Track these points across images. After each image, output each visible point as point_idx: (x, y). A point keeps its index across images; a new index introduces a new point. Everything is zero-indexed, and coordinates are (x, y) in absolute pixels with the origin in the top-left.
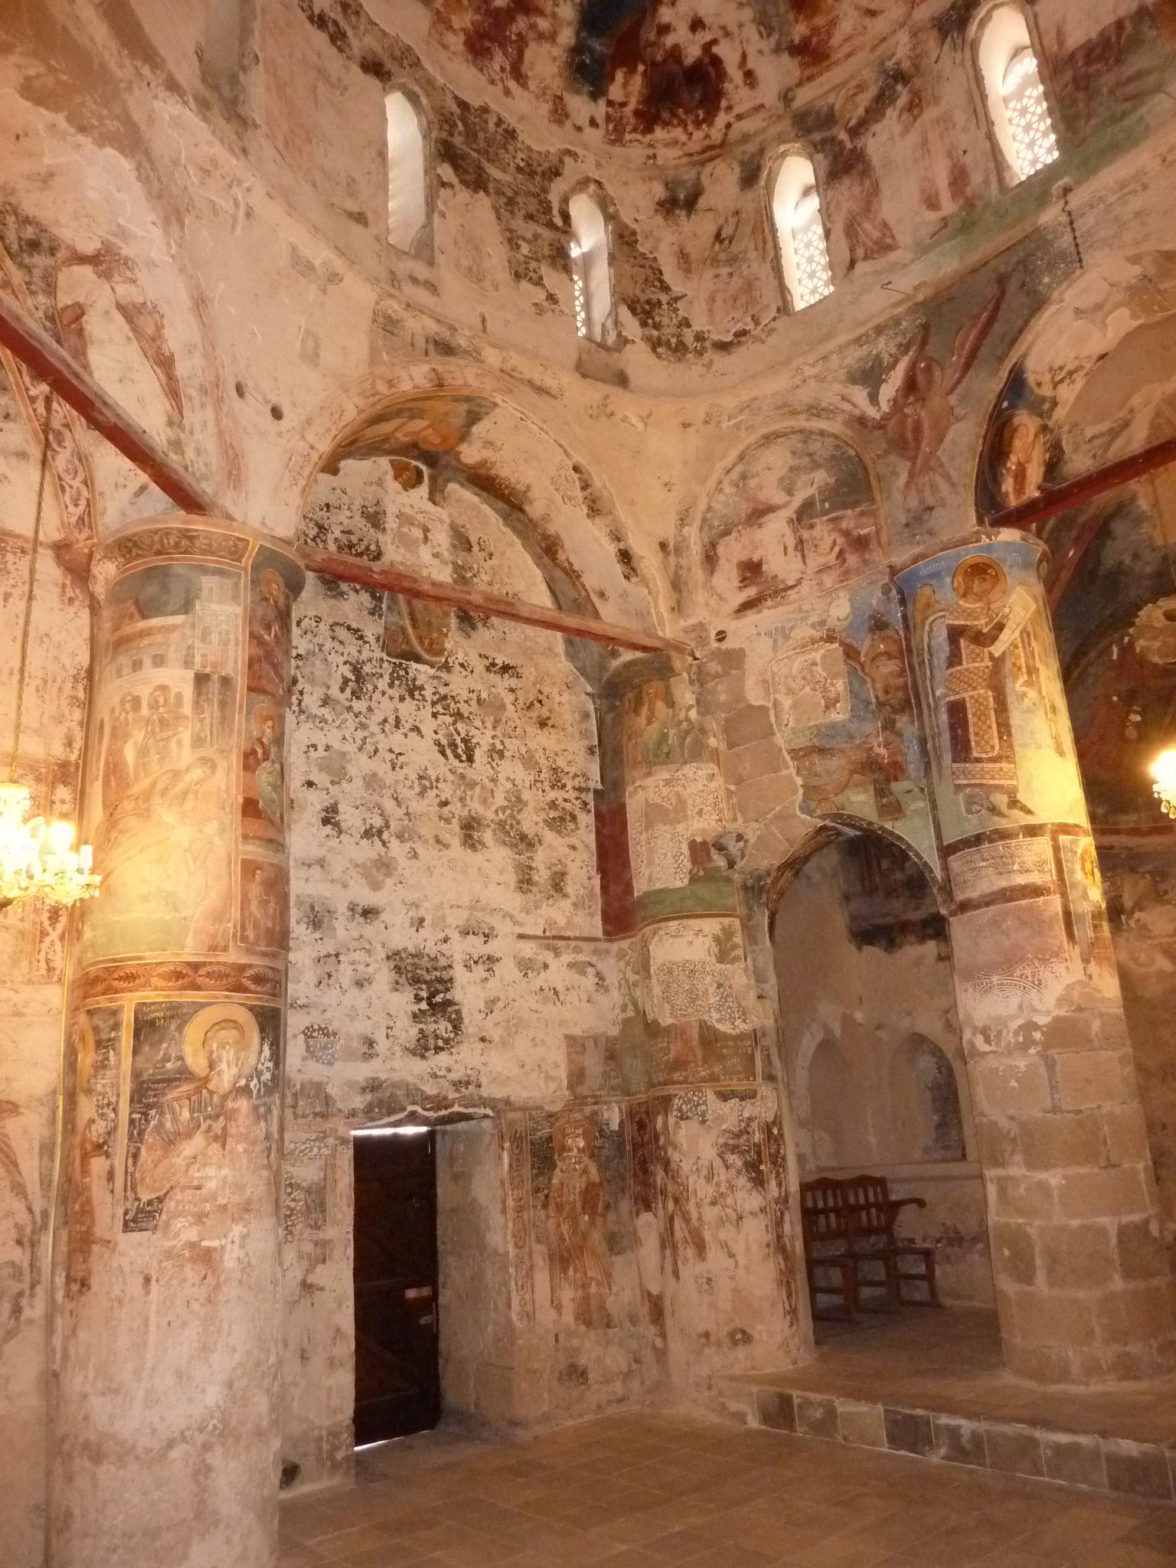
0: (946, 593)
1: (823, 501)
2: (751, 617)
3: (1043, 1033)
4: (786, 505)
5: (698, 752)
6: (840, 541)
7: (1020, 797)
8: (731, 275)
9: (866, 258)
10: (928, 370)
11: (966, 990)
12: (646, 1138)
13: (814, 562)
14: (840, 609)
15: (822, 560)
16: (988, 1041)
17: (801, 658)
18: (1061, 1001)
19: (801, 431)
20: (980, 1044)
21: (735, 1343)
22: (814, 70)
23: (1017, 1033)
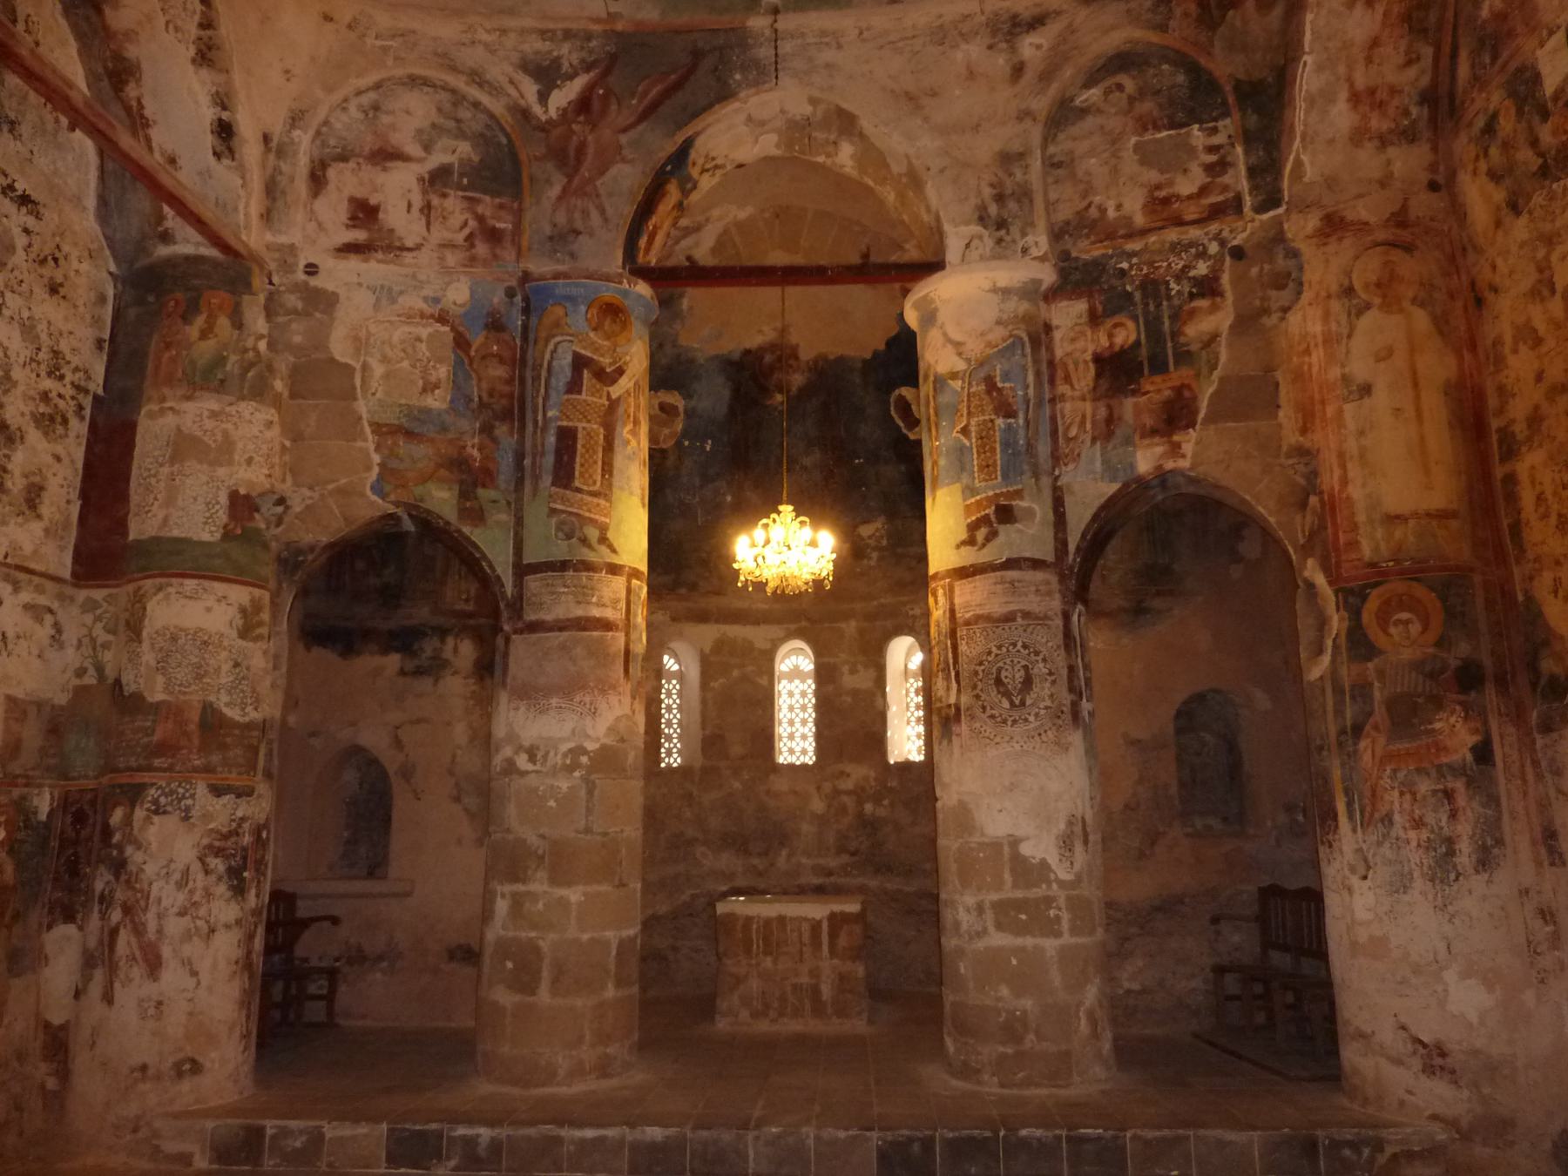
0: (579, 319)
1: (461, 175)
2: (354, 263)
3: (590, 758)
4: (420, 160)
5: (260, 392)
6: (472, 223)
7: (610, 535)
10: (605, 98)
11: (517, 709)
12: (84, 833)
13: (438, 234)
14: (458, 294)
15: (448, 235)
16: (532, 758)
17: (407, 329)
18: (611, 729)
19: (454, 91)
20: (522, 762)
21: (180, 1075)
23: (565, 755)
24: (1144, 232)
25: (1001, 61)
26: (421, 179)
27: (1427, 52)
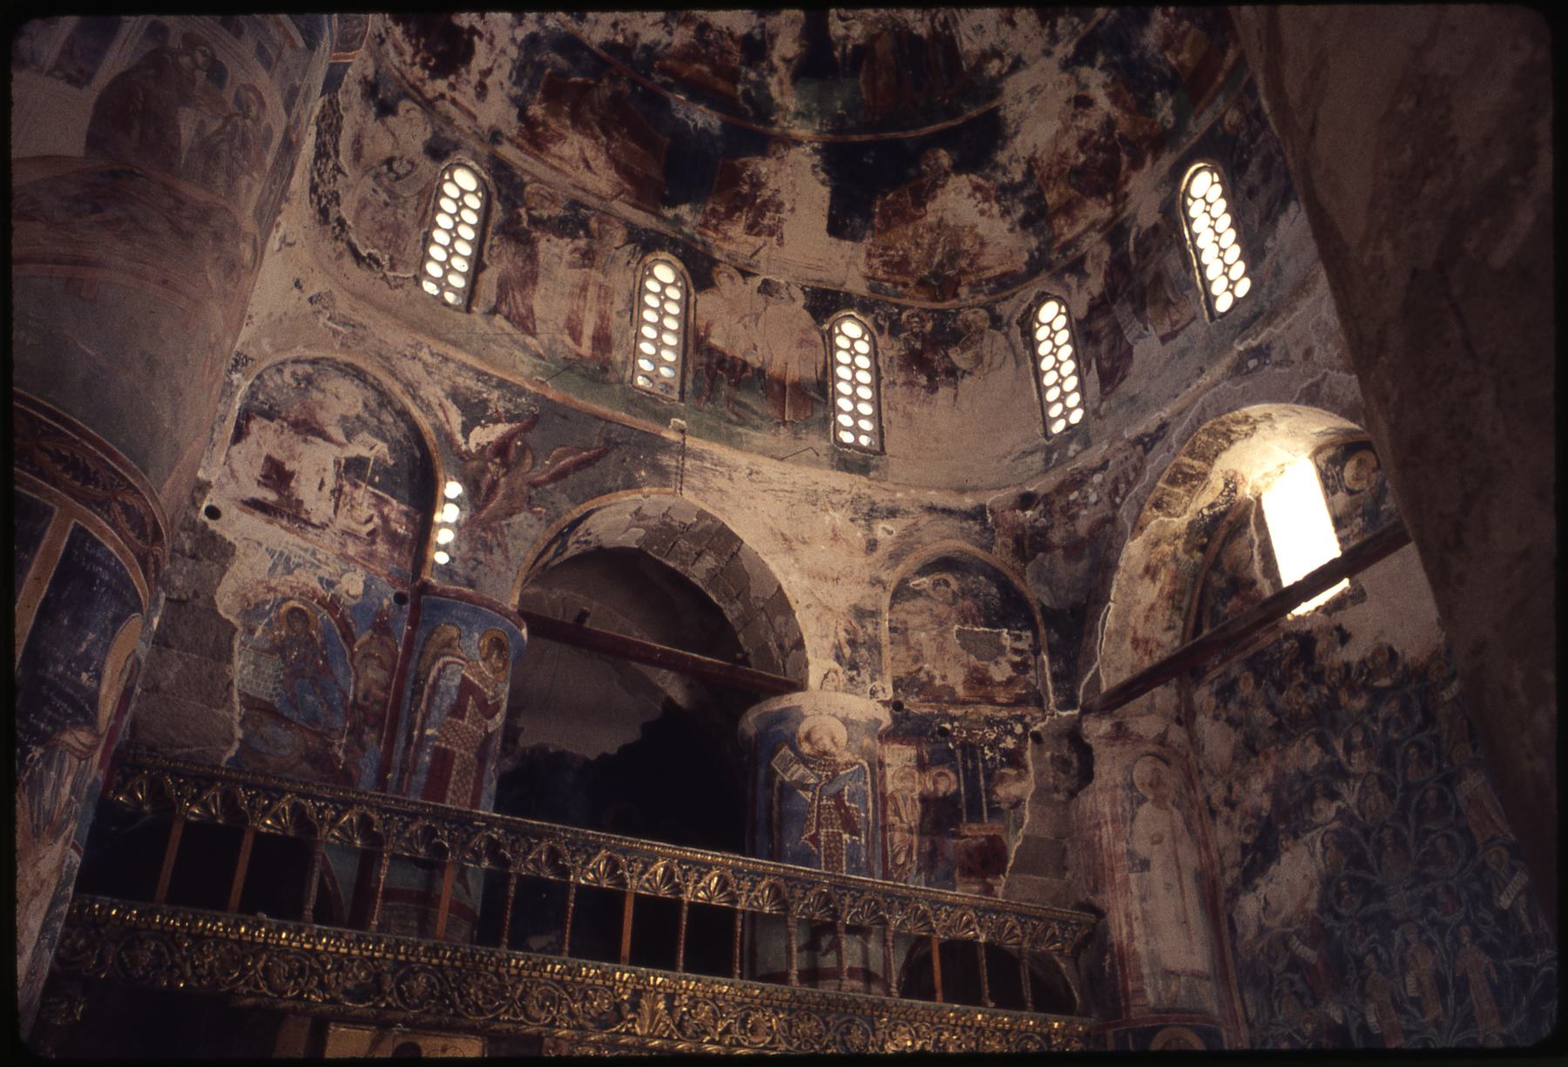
1: (374, 472)
4: (340, 445)
8: (386, 204)
9: (507, 318)
10: (522, 451)
22: (527, 146)
24: (964, 703)
25: (859, 534)
26: (337, 463)
27: (1180, 624)
